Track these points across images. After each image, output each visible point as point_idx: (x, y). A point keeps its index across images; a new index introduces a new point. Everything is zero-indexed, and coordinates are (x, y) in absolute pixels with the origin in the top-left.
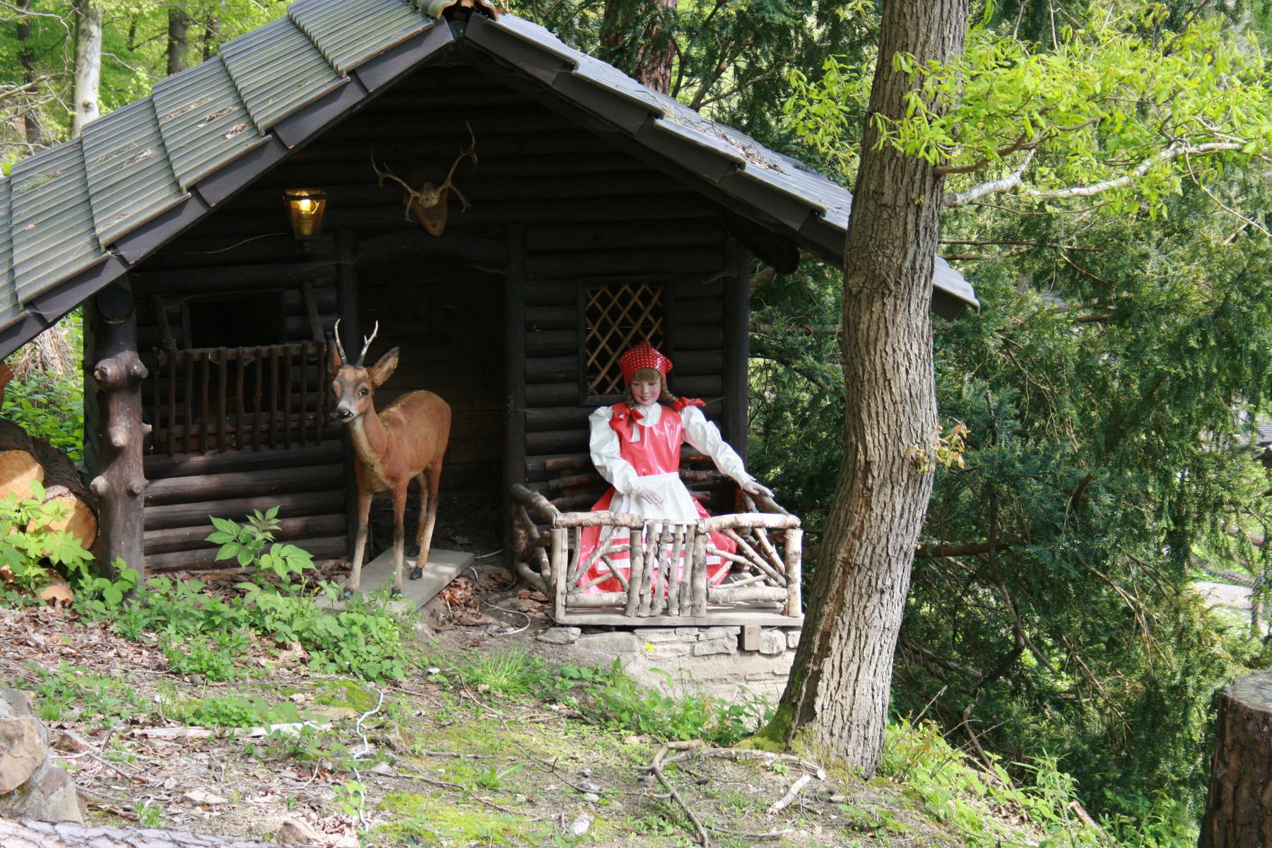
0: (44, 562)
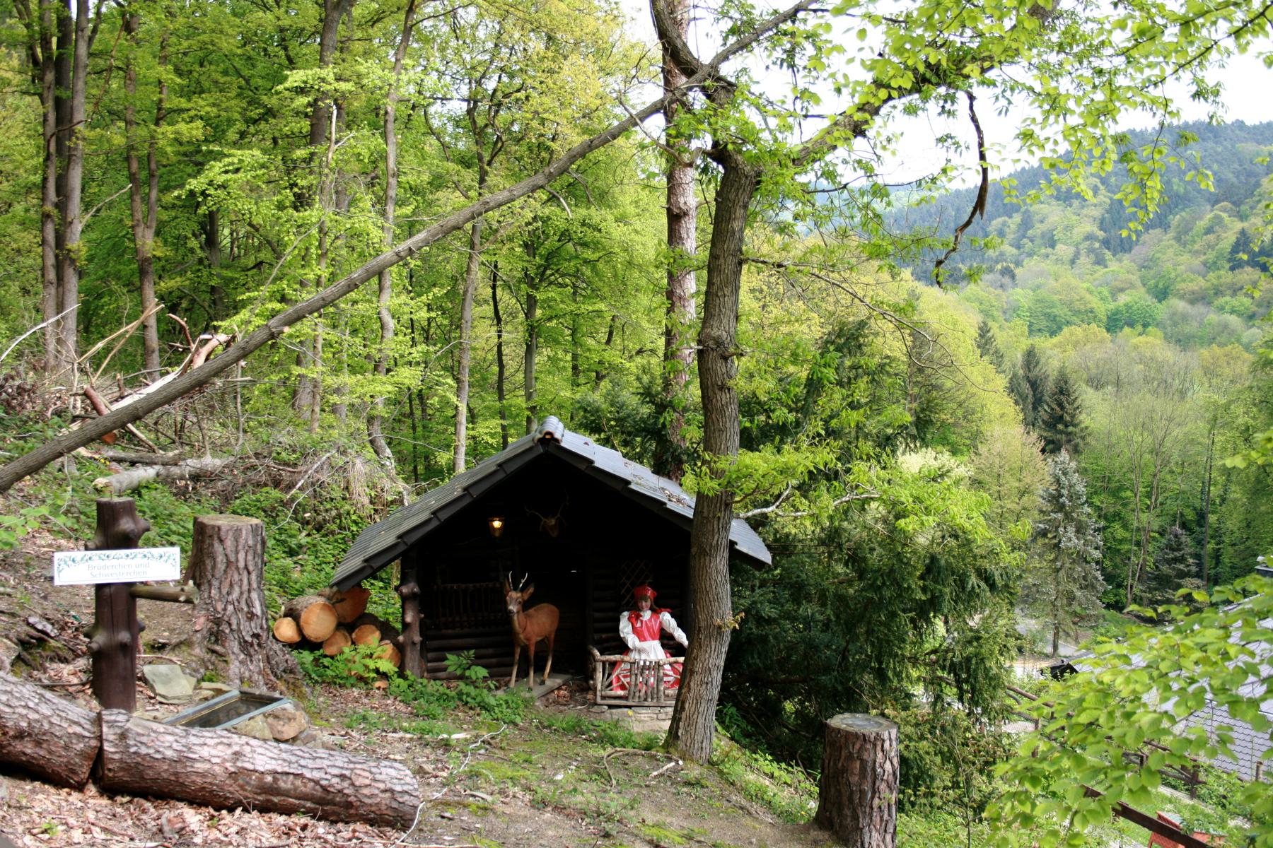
0: (377, 671)
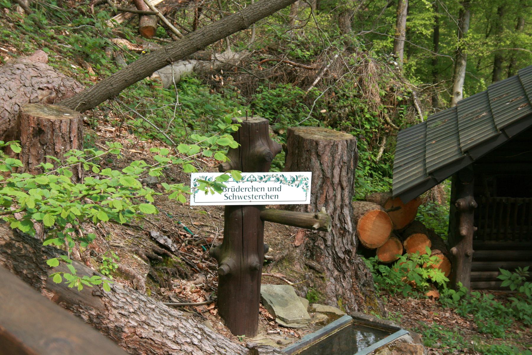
0: (429, 280)
